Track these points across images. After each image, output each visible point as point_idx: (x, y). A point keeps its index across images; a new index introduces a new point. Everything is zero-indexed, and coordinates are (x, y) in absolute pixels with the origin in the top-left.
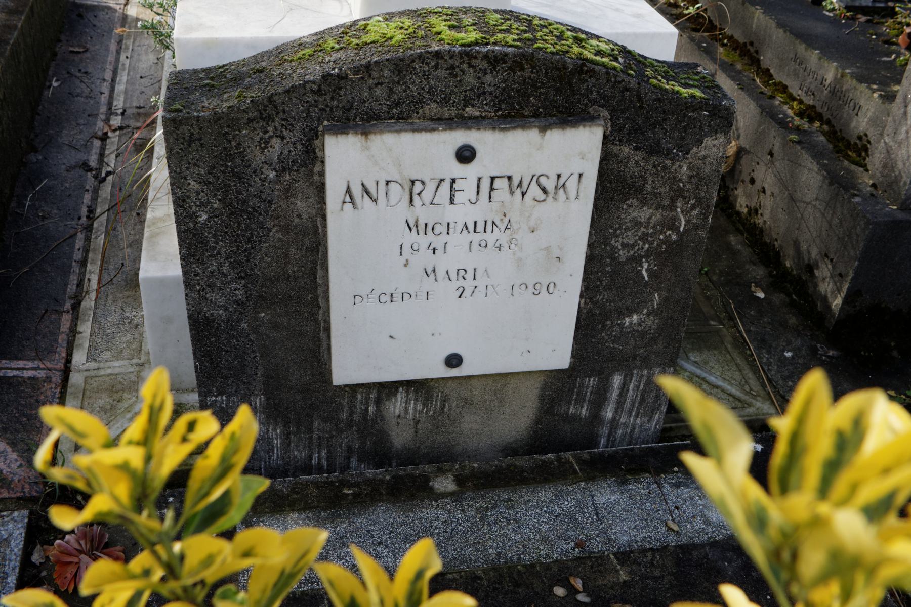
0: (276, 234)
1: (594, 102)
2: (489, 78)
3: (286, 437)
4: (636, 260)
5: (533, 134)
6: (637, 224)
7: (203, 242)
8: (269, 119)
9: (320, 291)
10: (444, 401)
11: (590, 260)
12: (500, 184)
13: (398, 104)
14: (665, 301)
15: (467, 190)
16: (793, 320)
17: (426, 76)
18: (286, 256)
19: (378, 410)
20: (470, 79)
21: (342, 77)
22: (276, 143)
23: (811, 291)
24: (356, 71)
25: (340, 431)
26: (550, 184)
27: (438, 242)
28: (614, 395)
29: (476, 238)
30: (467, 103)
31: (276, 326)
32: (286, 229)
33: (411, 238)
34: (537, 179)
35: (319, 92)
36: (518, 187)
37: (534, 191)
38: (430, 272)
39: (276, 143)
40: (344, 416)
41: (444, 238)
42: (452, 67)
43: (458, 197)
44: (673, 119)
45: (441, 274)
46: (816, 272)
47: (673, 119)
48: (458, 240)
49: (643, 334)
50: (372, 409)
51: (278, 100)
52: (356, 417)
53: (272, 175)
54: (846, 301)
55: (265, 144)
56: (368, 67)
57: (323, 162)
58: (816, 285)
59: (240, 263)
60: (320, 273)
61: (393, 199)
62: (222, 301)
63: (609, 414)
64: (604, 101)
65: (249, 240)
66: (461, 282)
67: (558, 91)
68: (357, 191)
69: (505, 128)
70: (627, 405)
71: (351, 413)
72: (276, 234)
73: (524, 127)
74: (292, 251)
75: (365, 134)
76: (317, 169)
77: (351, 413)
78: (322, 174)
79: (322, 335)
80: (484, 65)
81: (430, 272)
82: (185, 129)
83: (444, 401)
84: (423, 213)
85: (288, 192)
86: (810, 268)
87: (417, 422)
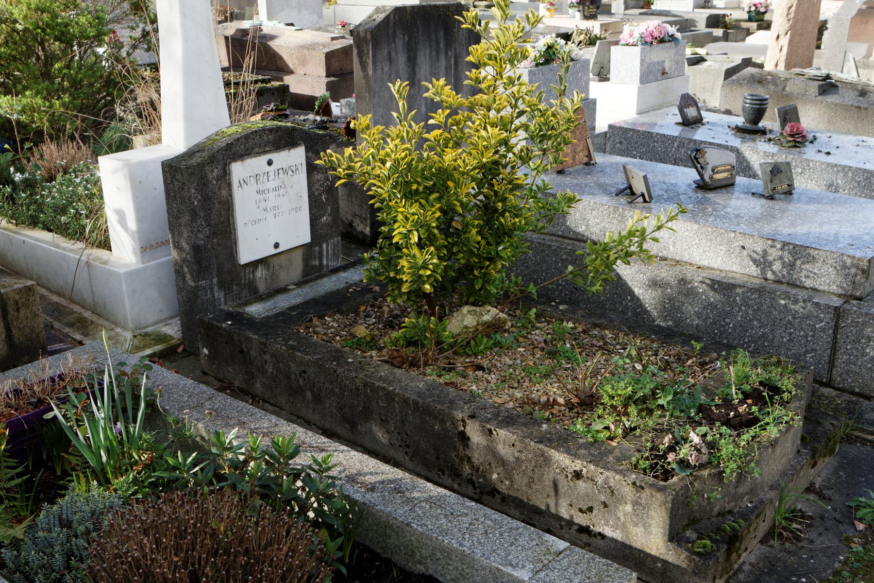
0: (217, 206)
1: (298, 139)
2: (270, 137)
3: (225, 296)
4: (320, 195)
5: (287, 151)
6: (318, 181)
7: (196, 213)
8: (213, 162)
9: (231, 226)
10: (273, 267)
11: (309, 196)
12: (281, 171)
13: (247, 150)
14: (332, 209)
15: (271, 174)
16: (353, 246)
17: (254, 139)
18: (221, 214)
19: (254, 277)
20: (265, 138)
21: (232, 144)
22: (215, 170)
23: (354, 233)
24: (235, 141)
25: (242, 289)
26: (293, 169)
27: (266, 197)
28: (325, 253)
29: (276, 193)
30: (266, 146)
31: (219, 244)
32: (220, 203)
33: (259, 197)
34: (290, 167)
35: (226, 150)
36: (285, 172)
37: (290, 172)
38: (265, 210)
39: (215, 170)
40: (243, 282)
41: (268, 195)
42: (260, 135)
43: (270, 179)
44: (320, 141)
45: (268, 209)
46: (354, 225)
47: (320, 141)
48: (272, 195)
49: (328, 224)
50: (251, 276)
51: (215, 155)
52: (247, 282)
53: (215, 182)
54: (371, 228)
55: (212, 171)
56: (238, 139)
57: (229, 175)
58: (356, 230)
59: (207, 219)
60: (231, 219)
61: (252, 183)
62: (202, 237)
63: (325, 262)
64: (302, 139)
65: (210, 210)
66: (275, 212)
67: (289, 138)
68: (242, 182)
69: (84, 307)
70: (330, 257)
71: (245, 280)
72: (217, 206)
73: (284, 150)
74: (222, 211)
75: (242, 160)
76: (228, 177)
77: (245, 280)
78: (229, 179)
79: (234, 245)
80: (268, 132)
81: (265, 210)
82: (190, 170)
83: (273, 267)
84: (261, 187)
85: (220, 188)
86: (350, 225)
87: (266, 279)
